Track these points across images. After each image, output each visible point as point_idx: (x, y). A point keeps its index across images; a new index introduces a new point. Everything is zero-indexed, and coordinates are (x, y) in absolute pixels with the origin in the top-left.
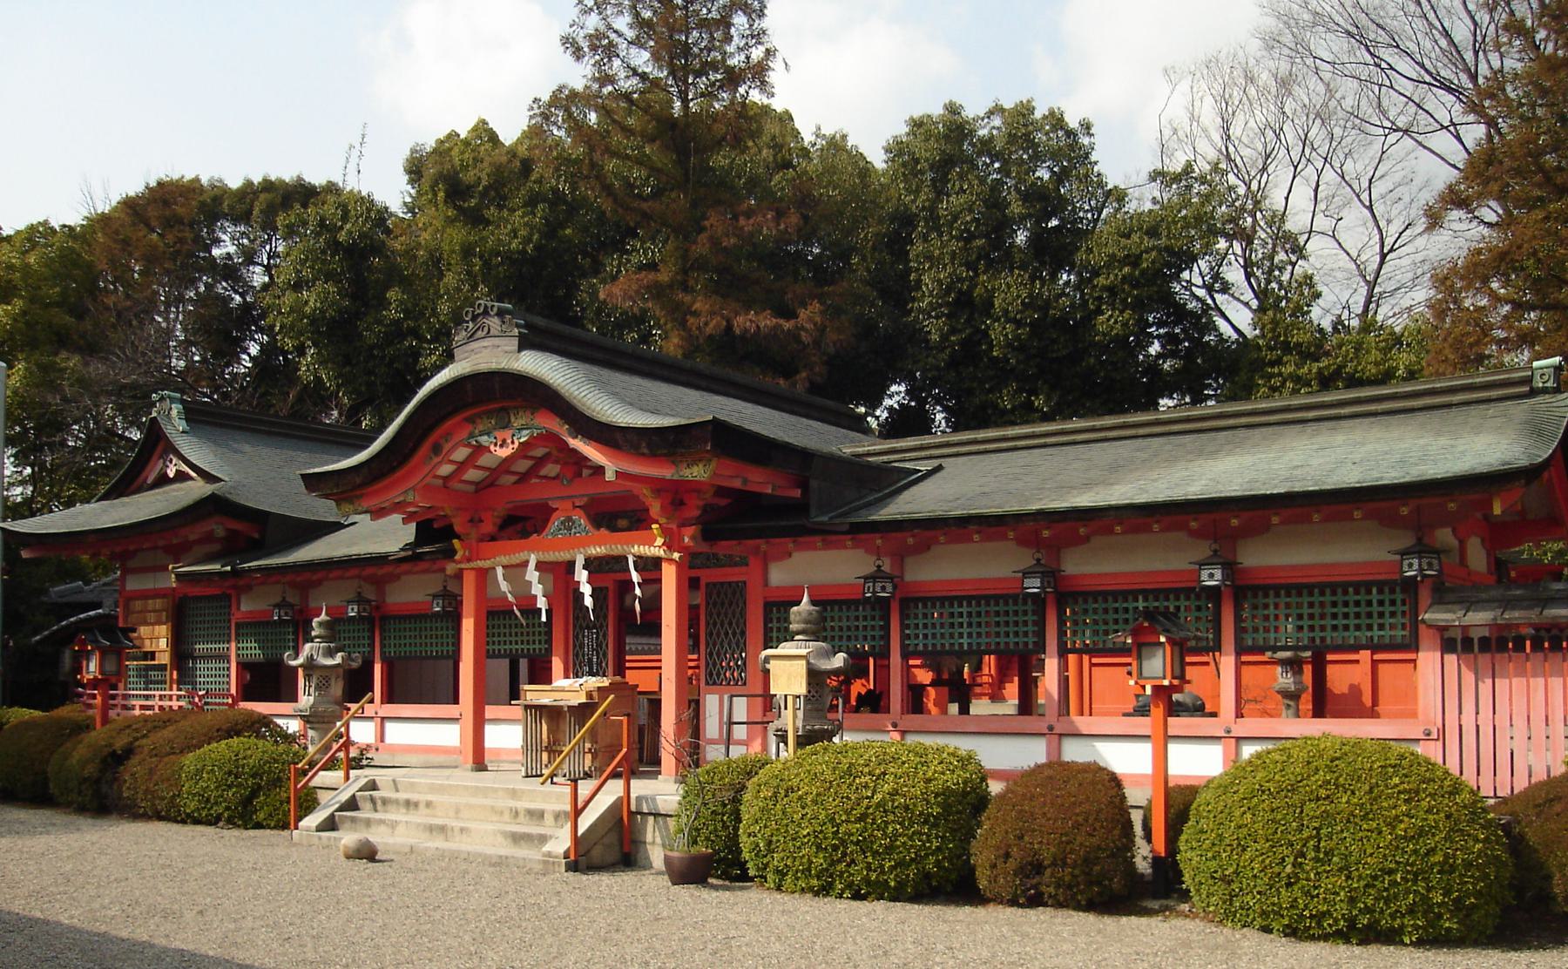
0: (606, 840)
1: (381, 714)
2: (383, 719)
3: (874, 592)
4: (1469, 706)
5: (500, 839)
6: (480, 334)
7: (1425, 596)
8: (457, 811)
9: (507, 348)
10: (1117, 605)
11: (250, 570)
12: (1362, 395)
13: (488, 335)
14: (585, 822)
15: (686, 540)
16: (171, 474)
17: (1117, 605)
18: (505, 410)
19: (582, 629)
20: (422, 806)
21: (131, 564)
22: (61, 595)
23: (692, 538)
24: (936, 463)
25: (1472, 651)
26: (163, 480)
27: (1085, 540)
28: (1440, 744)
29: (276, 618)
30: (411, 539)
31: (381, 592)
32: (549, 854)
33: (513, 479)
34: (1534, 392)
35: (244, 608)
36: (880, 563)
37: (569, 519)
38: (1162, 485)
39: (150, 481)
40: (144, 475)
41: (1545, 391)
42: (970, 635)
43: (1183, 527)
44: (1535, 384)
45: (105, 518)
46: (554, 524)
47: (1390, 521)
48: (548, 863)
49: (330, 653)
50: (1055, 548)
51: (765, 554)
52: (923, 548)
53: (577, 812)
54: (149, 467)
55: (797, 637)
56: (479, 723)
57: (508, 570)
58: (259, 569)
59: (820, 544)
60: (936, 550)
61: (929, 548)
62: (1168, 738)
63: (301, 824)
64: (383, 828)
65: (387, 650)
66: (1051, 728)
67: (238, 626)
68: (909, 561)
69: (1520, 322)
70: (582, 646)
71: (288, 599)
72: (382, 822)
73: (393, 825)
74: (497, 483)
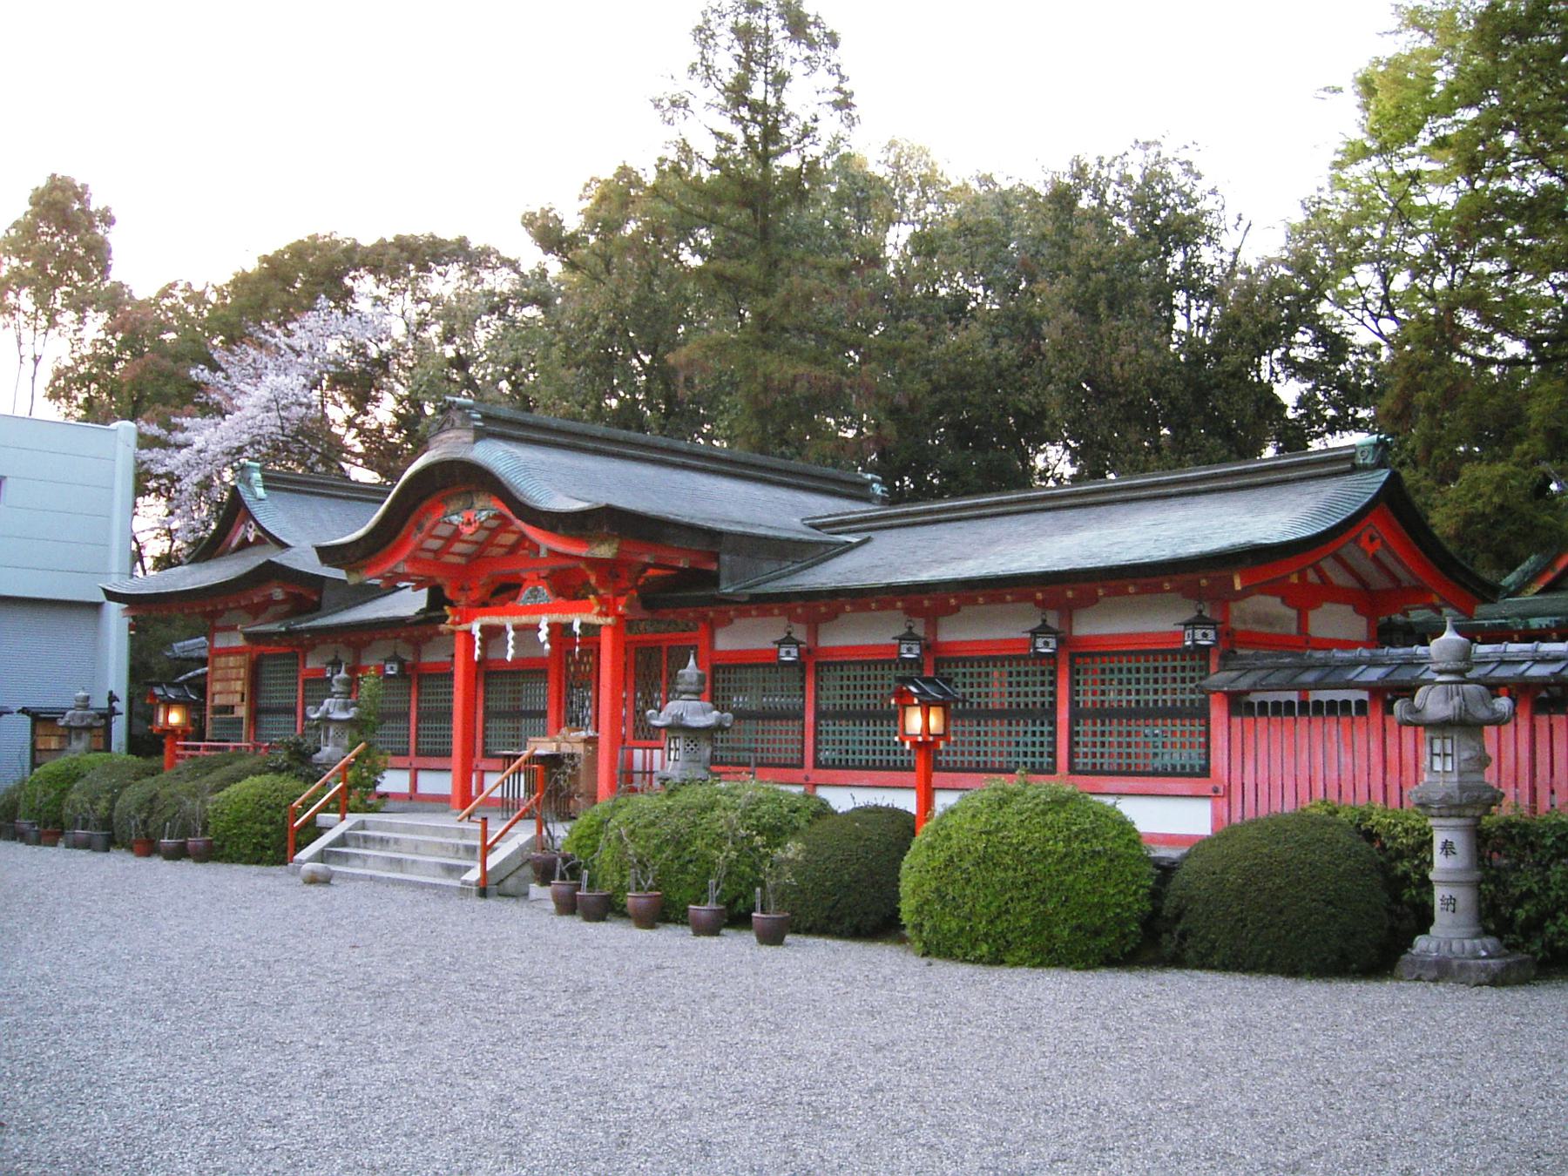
0: (521, 872)
1: (414, 766)
2: (483, 771)
3: (1194, 641)
4: (1249, 767)
5: (439, 871)
6: (447, 426)
7: (1214, 662)
8: (416, 847)
9: (466, 439)
10: (1175, 664)
11: (302, 631)
12: (899, 510)
13: (453, 427)
14: (493, 860)
15: (620, 609)
16: (251, 540)
17: (1175, 664)
18: (469, 493)
19: (572, 687)
20: (392, 842)
21: (219, 623)
22: (183, 649)
23: (629, 606)
24: (865, 535)
25: (1266, 714)
26: (245, 544)
27: (957, 609)
28: (1225, 799)
29: (1188, 643)
30: (424, 605)
31: (418, 653)
32: (465, 882)
33: (502, 551)
34: (1355, 469)
35: (309, 666)
36: (1201, 607)
37: (536, 590)
38: (1034, 558)
39: (234, 544)
40: (228, 539)
41: (1365, 468)
42: (1138, 692)
43: (1030, 598)
44: (1357, 462)
45: (189, 580)
46: (526, 593)
47: (1192, 593)
48: (463, 891)
49: (346, 708)
50: (1068, 611)
51: (712, 621)
52: (832, 616)
53: (487, 849)
54: (231, 533)
55: (684, 697)
56: (467, 771)
57: (521, 633)
58: (309, 630)
59: (776, 611)
60: (842, 617)
61: (836, 617)
62: (417, 770)
63: (296, 857)
64: (358, 862)
65: (1081, 698)
66: (807, 779)
67: (305, 682)
68: (822, 627)
69: (1028, 443)
70: (571, 703)
71: (915, 630)
72: (357, 855)
73: (365, 858)
74: (485, 554)
